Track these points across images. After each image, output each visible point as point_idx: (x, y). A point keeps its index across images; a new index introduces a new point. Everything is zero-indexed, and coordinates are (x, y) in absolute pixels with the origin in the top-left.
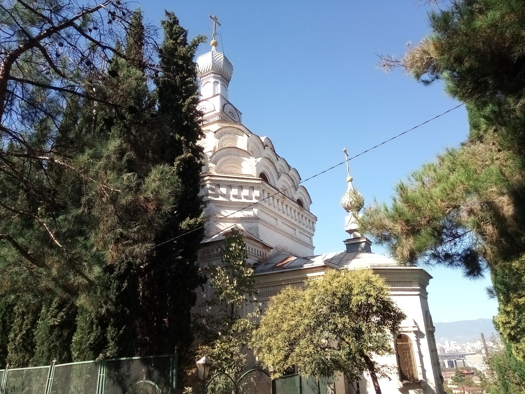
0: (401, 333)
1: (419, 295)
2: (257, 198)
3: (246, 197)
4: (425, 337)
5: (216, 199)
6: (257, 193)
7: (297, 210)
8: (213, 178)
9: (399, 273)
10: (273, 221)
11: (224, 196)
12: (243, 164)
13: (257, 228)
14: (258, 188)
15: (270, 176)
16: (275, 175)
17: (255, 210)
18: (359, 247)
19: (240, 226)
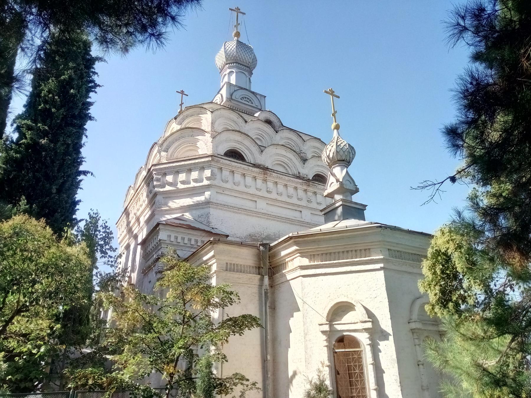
0: (345, 334)
1: (381, 269)
2: (208, 179)
3: (195, 181)
4: (391, 338)
5: (162, 190)
6: (208, 173)
7: (299, 186)
8: (157, 167)
9: (342, 238)
10: (249, 205)
11: (170, 184)
12: (199, 144)
13: (208, 215)
14: (209, 167)
15: (247, 152)
16: (255, 150)
17: (207, 194)
18: (335, 214)
19: (188, 216)
